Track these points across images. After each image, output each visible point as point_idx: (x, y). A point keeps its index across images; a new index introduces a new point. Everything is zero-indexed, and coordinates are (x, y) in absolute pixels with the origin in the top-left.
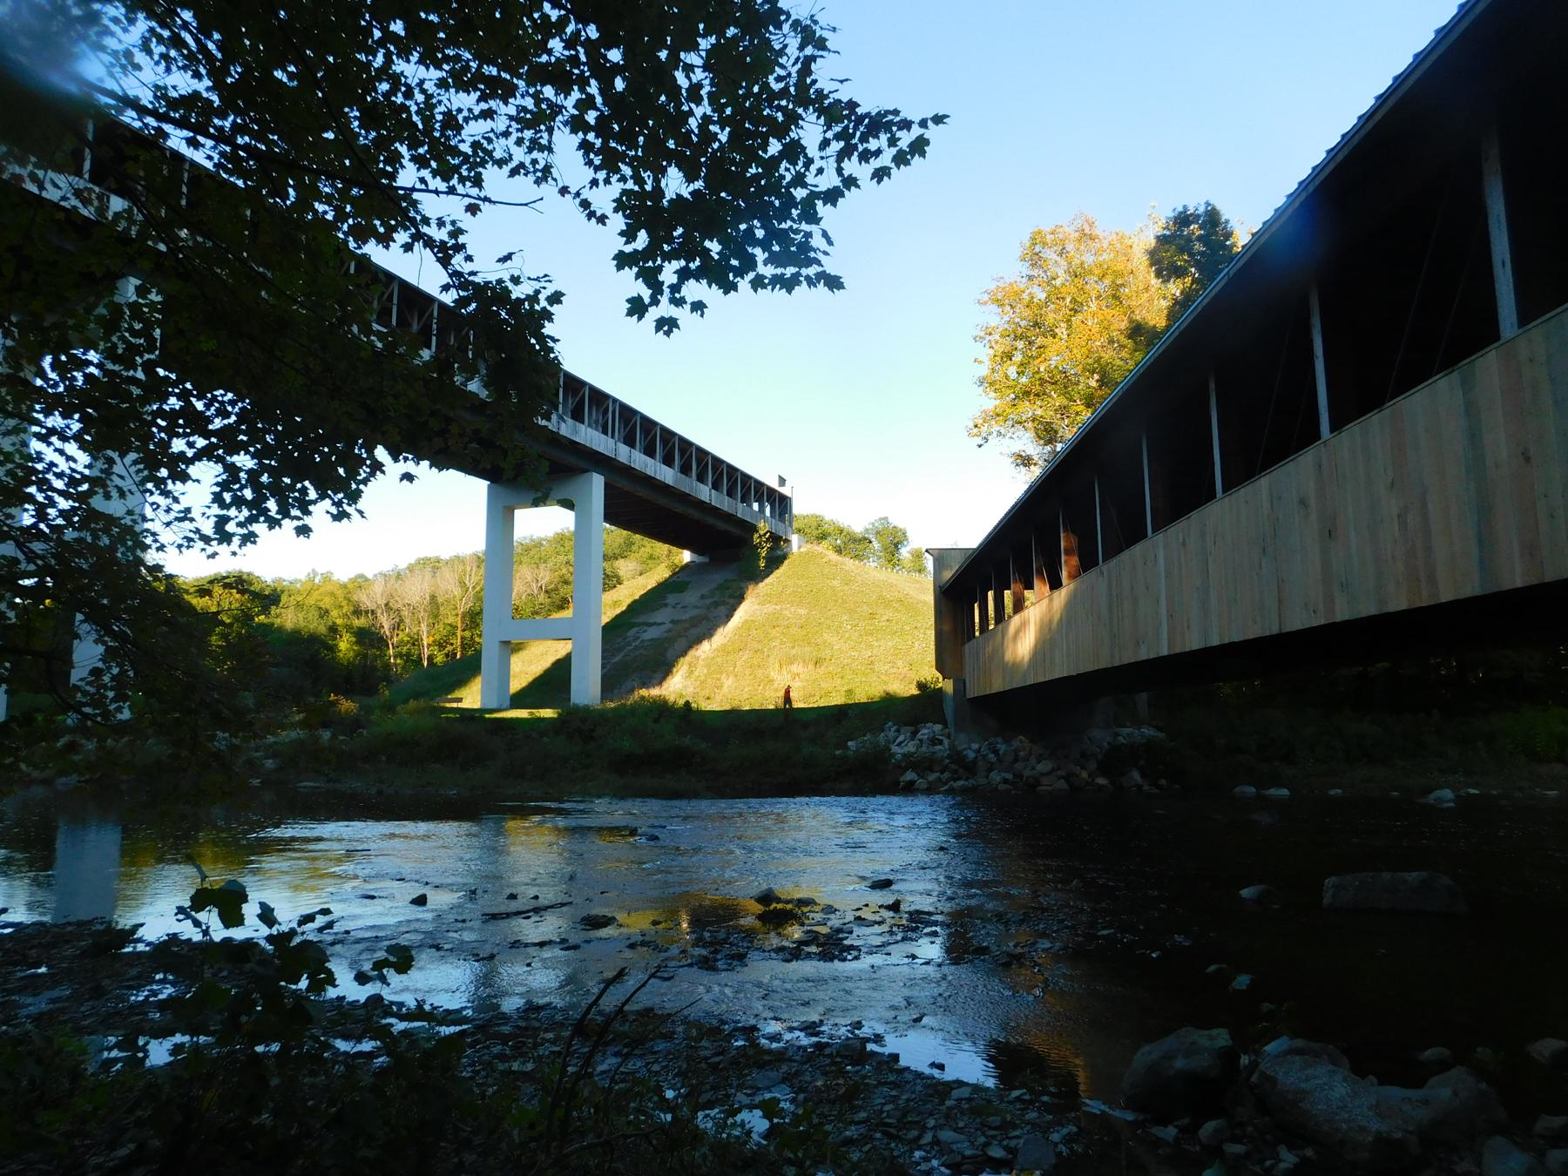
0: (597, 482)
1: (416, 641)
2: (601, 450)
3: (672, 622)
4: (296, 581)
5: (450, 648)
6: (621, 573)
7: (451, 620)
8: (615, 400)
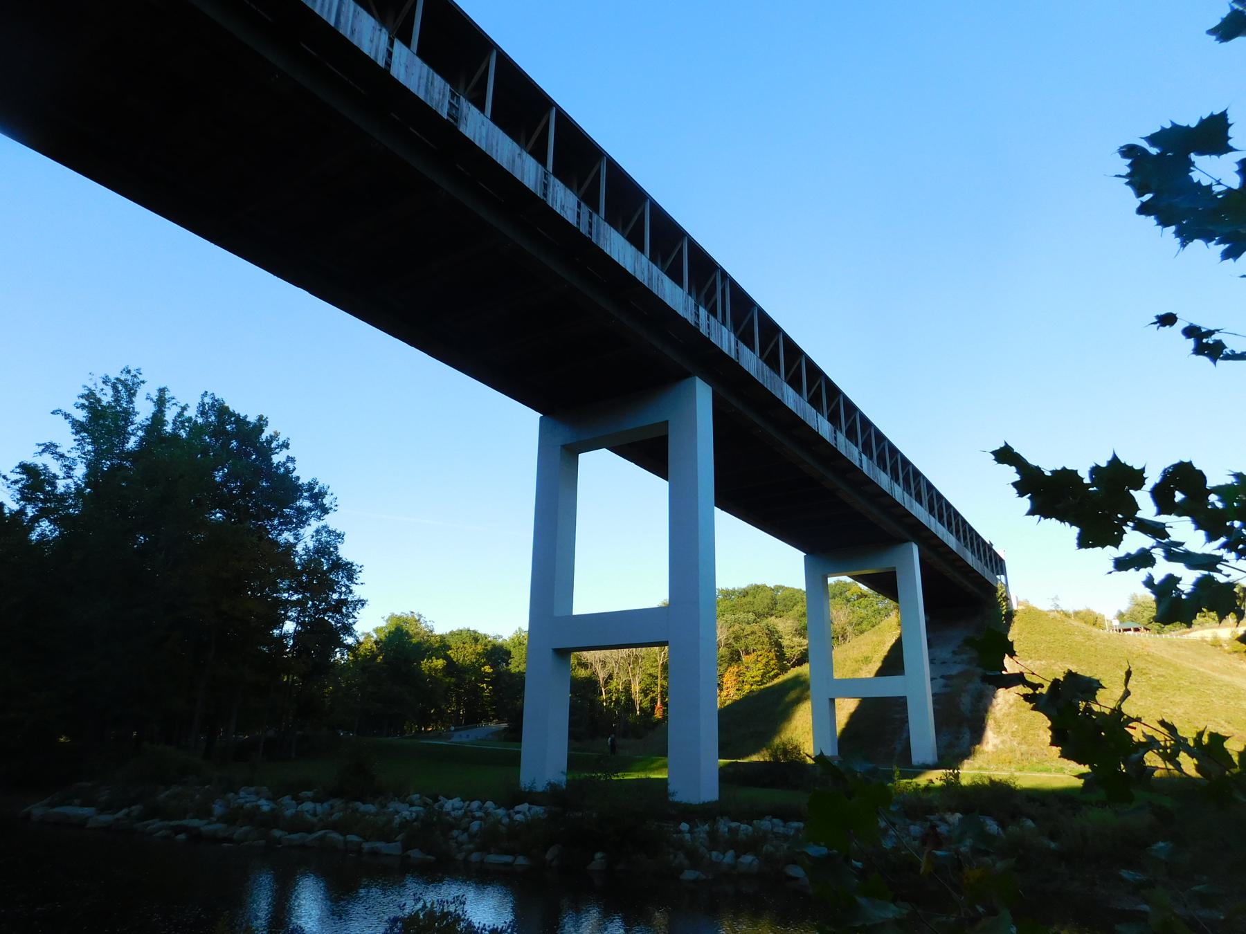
0: (703, 395)
1: (627, 689)
2: (366, 49)
3: (942, 677)
4: (500, 637)
5: (652, 695)
6: (779, 629)
7: (651, 671)
8: (725, 275)
